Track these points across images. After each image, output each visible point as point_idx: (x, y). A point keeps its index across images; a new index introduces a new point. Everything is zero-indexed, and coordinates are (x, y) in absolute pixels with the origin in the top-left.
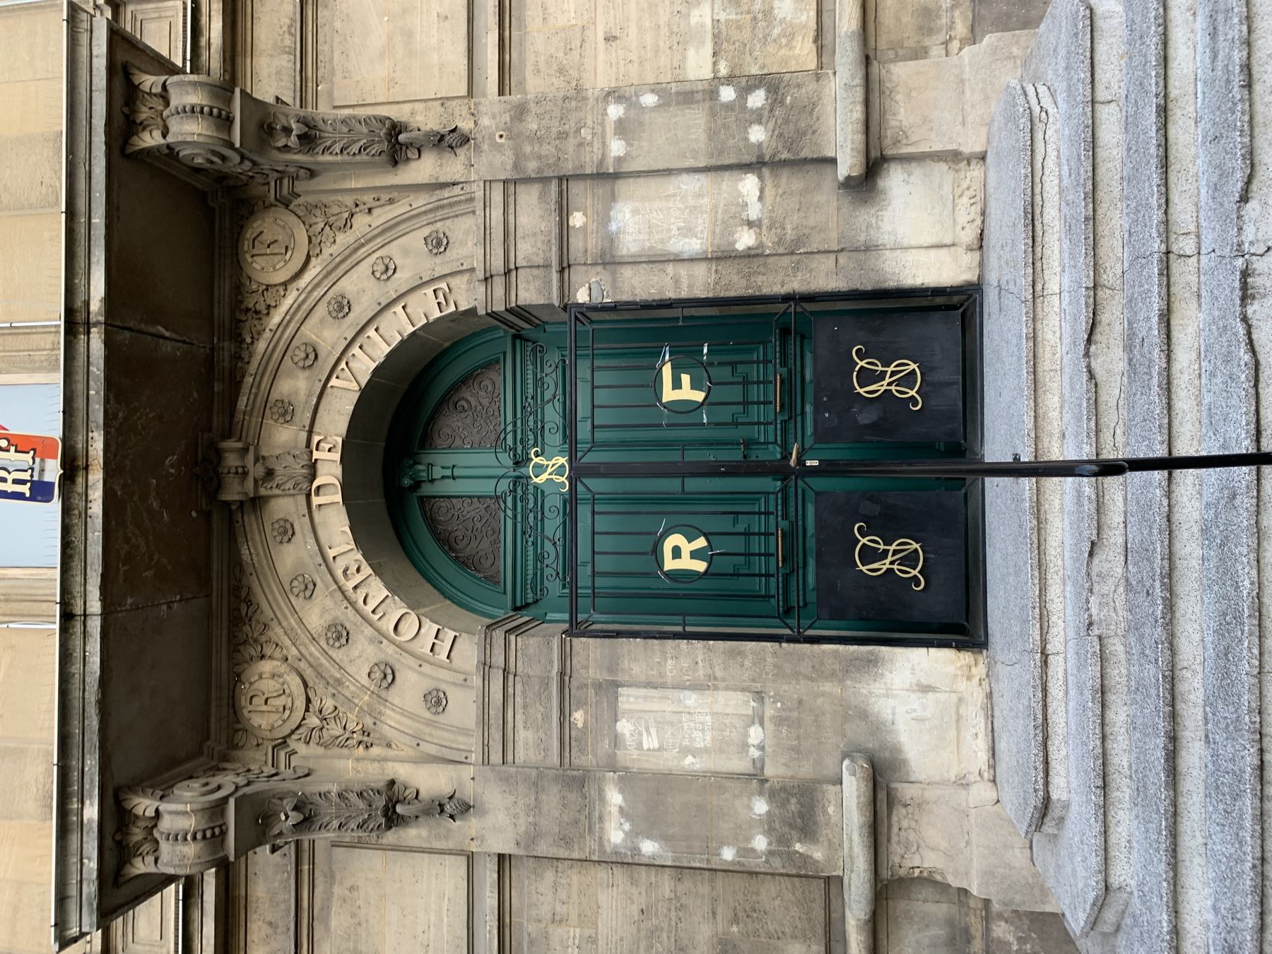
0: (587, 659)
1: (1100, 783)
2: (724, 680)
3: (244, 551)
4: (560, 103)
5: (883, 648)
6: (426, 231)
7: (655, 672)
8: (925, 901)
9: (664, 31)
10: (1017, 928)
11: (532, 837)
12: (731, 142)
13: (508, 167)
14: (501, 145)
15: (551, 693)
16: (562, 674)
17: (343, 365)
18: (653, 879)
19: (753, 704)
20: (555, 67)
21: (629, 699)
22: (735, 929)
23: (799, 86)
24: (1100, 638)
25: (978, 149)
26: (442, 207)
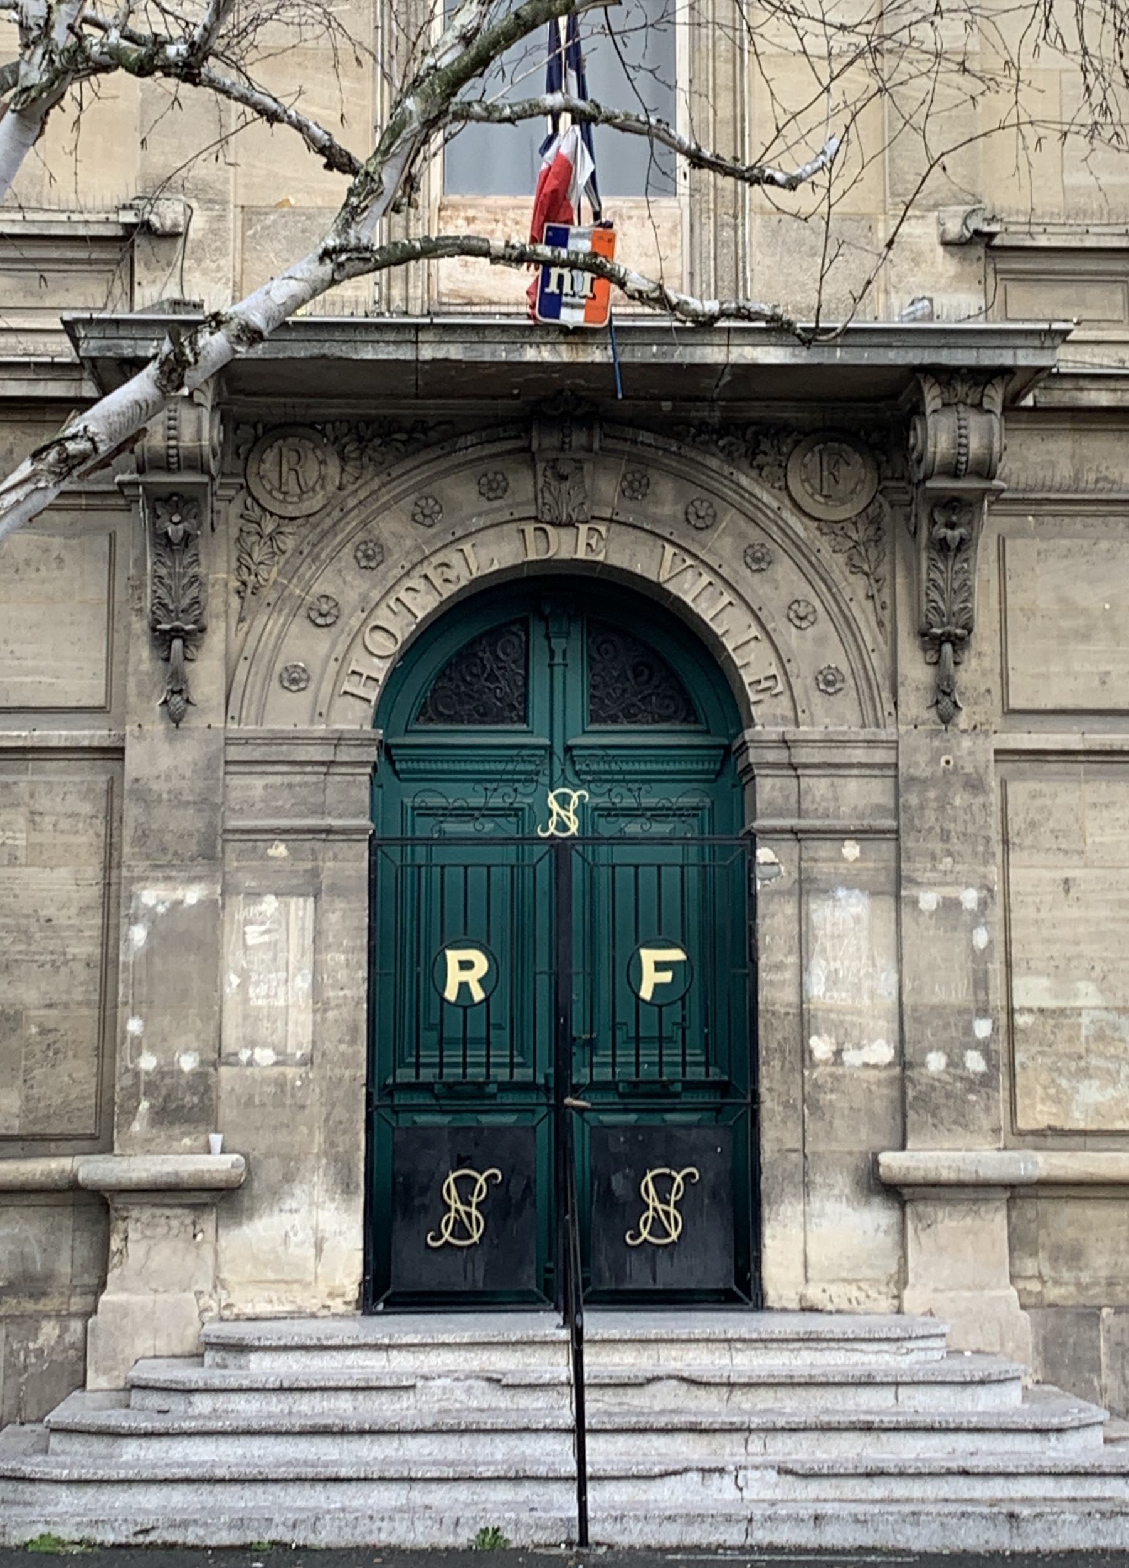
0: (344, 860)
1: (286, 1385)
2: (324, 1020)
3: (471, 439)
4: (983, 833)
5: (362, 1200)
6: (845, 669)
7: (331, 939)
8: (73, 1249)
9: (1071, 950)
10: (53, 1348)
11: (144, 797)
12: (929, 1032)
13: (912, 771)
14: (938, 763)
15: (306, 817)
16: (329, 831)
17: (689, 562)
18: (87, 933)
19: (299, 1054)
20: (1037, 817)
21: (301, 909)
22: (34, 1030)
23: (987, 1109)
24: (414, 1387)
25: (906, 1306)
26: (870, 688)
